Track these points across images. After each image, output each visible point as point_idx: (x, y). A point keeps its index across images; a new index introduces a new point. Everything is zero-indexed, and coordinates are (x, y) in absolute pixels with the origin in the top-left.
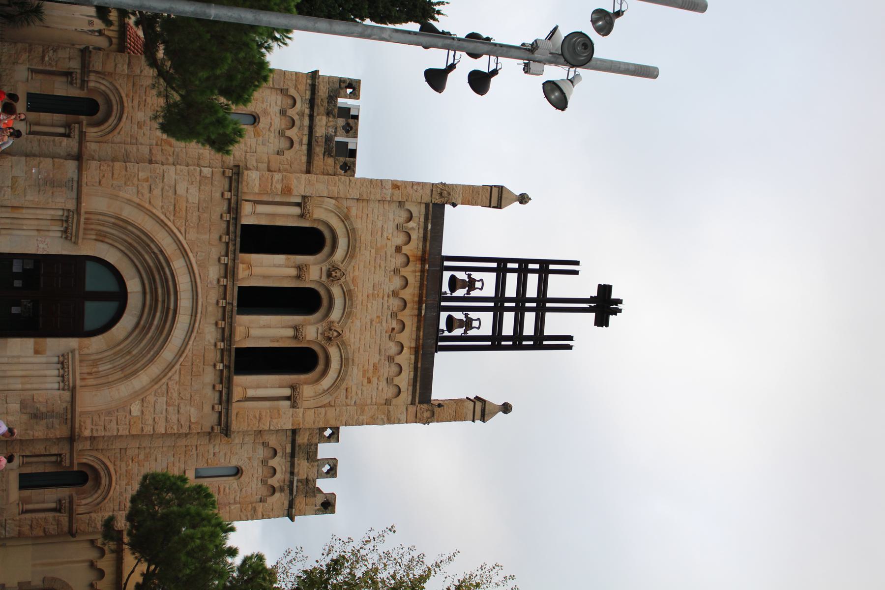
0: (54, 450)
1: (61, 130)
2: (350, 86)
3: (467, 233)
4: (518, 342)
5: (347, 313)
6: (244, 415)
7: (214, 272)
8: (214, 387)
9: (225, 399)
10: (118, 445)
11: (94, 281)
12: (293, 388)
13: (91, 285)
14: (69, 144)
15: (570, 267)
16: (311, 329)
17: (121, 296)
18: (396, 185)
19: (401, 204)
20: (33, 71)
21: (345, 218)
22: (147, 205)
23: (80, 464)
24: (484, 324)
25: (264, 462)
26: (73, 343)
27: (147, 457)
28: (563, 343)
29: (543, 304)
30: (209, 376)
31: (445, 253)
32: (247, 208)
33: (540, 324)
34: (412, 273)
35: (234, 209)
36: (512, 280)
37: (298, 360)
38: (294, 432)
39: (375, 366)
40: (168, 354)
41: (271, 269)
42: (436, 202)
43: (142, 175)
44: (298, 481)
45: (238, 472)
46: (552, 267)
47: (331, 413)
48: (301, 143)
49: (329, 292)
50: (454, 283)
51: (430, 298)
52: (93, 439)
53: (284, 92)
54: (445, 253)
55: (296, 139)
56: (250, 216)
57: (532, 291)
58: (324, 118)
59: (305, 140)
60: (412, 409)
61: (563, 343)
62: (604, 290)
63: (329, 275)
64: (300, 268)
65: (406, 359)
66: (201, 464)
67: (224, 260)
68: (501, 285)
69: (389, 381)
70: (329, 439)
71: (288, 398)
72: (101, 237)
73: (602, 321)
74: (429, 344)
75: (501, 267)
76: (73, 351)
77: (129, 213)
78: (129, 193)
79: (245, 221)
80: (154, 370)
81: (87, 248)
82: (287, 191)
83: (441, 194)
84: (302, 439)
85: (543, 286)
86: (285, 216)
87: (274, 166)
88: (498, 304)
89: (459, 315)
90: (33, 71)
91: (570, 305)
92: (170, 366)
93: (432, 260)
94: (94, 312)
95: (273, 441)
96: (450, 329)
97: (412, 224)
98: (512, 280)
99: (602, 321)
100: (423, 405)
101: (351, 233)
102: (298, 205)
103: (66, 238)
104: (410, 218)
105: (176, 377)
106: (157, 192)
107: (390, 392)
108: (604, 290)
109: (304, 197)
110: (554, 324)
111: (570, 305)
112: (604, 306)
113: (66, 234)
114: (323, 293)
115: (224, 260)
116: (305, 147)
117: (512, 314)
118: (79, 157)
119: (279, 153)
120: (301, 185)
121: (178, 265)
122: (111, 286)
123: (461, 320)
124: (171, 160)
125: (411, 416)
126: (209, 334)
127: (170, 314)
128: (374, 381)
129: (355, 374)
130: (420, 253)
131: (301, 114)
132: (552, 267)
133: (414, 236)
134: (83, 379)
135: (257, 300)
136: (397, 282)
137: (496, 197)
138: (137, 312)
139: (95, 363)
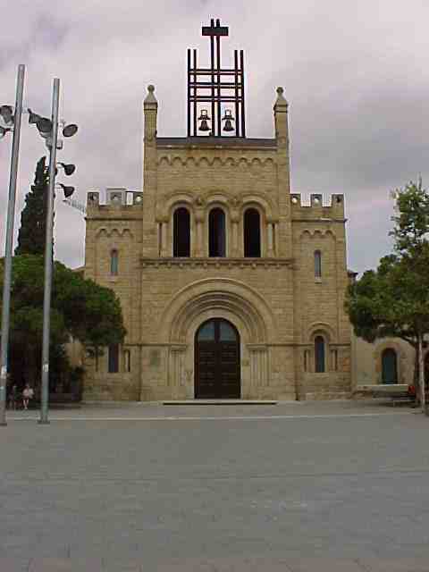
0: (302, 354)
1: (127, 355)
2: (92, 198)
3: (173, 124)
4: (239, 86)
5: (223, 193)
6: (286, 251)
7: (200, 270)
8: (242, 268)
9: (274, 263)
10: (300, 321)
11: (208, 336)
12: (267, 223)
13: (211, 337)
14: (133, 350)
15: (191, 55)
16: (234, 213)
17: (217, 322)
18: (146, 168)
19: (157, 164)
20: (97, 370)
21: (167, 197)
22: (163, 310)
23: (311, 340)
24: (228, 108)
25: (312, 237)
26: (243, 346)
27: (307, 304)
28: (239, 56)
29: (215, 71)
30: (260, 271)
31: (186, 136)
32: (164, 254)
33: (227, 73)
34: (198, 155)
35: (165, 262)
36: (200, 92)
37: (252, 220)
38: (293, 221)
39: (254, 175)
40: (248, 295)
41: (199, 238)
42: (155, 142)
43: (148, 311)
44: (324, 217)
45: (318, 253)
46: (192, 67)
47: (282, 199)
48: (126, 225)
49: (211, 204)
50: (204, 128)
51: (214, 143)
52: (296, 334)
53: (98, 236)
54: (186, 136)
55: (123, 228)
56: (168, 251)
57: (208, 79)
58: (110, 212)
59: (124, 222)
60: (279, 151)
61: (239, 56)
62: (206, 31)
63: (200, 204)
64: (232, 222)
65: (249, 156)
66: (313, 273)
67: (193, 265)
68: (204, 99)
69: (262, 165)
70: (299, 199)
71: (273, 226)
72: (184, 333)
73: (225, 31)
74: (242, 142)
75: (193, 99)
76: (248, 345)
77: (169, 319)
78: (158, 319)
79: (172, 255)
80: (256, 301)
81: (191, 340)
82: (153, 232)
83: (151, 141)
84: (298, 215)
85: (204, 72)
86: (168, 231)
87: (139, 239)
88: (216, 100)
89: (223, 124)
90: (97, 370)
91: (215, 52)
92: (254, 293)
93: (190, 143)
94: (226, 336)
95: (299, 233)
96: (207, 129)
97: (169, 158)
98: (200, 92)
99: (225, 31)
100: (275, 145)
101: (176, 193)
102: (161, 225)
103: (185, 350)
104: (166, 158)
105: (261, 290)
106: (156, 303)
107: (269, 164)
108: (206, 31)
109: (157, 221)
110: (227, 63)
111: (215, 52)
112: (215, 31)
113: (182, 350)
114: (211, 207)
115: (193, 265)
116: (128, 222)
117: (210, 94)
118: (140, 346)
119: (132, 236)
120: (149, 223)
121: (197, 291)
122: (211, 326)
123: (202, 123)
124: (139, 297)
125: (285, 151)
126: (236, 271)
127: (234, 297)
128: (264, 174)
129: (259, 187)
130: (187, 151)
131: (110, 225)
132: (192, 67)
133: (177, 155)
134: (262, 340)
135: (216, 247)
136: (204, 164)
137: (151, 107)
138: (220, 311)
139: (254, 335)
